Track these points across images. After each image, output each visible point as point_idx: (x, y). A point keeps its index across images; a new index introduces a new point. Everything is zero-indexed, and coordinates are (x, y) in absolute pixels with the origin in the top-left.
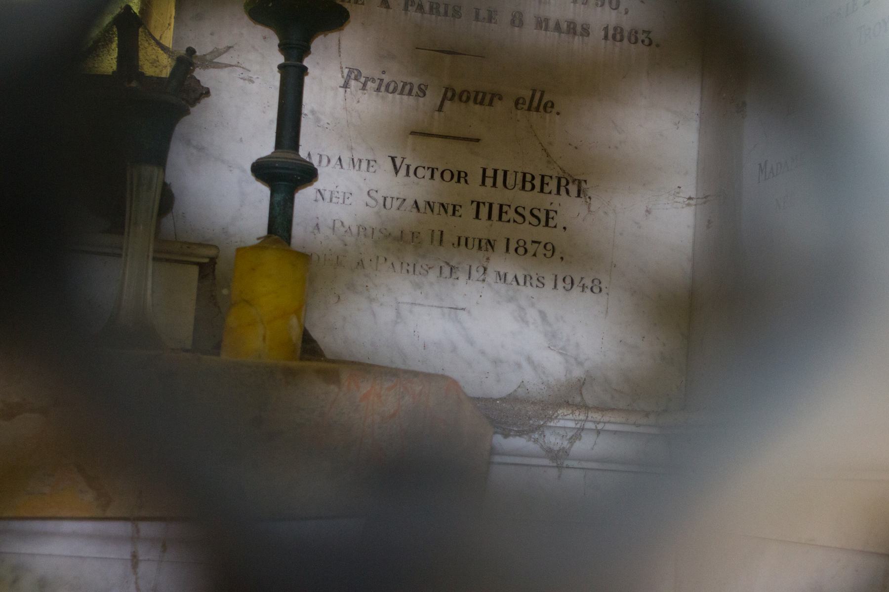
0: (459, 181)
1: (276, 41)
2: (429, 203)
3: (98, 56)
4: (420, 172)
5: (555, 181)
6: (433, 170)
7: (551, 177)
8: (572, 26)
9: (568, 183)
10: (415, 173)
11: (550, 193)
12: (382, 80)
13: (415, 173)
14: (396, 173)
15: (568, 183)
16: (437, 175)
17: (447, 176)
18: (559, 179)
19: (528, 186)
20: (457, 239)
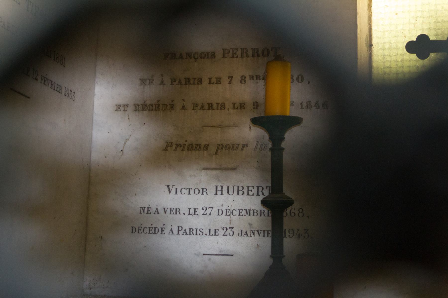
0: (203, 194)
1: (432, 38)
2: (164, 208)
3: (385, 73)
4: (183, 191)
5: (256, 189)
6: (189, 189)
7: (253, 187)
8: (211, 105)
9: (263, 189)
10: (199, 191)
11: (253, 195)
12: (185, 145)
13: (199, 191)
14: (170, 193)
15: (263, 189)
16: (192, 192)
17: (197, 191)
18: (258, 187)
19: (241, 193)
20: (240, 231)
